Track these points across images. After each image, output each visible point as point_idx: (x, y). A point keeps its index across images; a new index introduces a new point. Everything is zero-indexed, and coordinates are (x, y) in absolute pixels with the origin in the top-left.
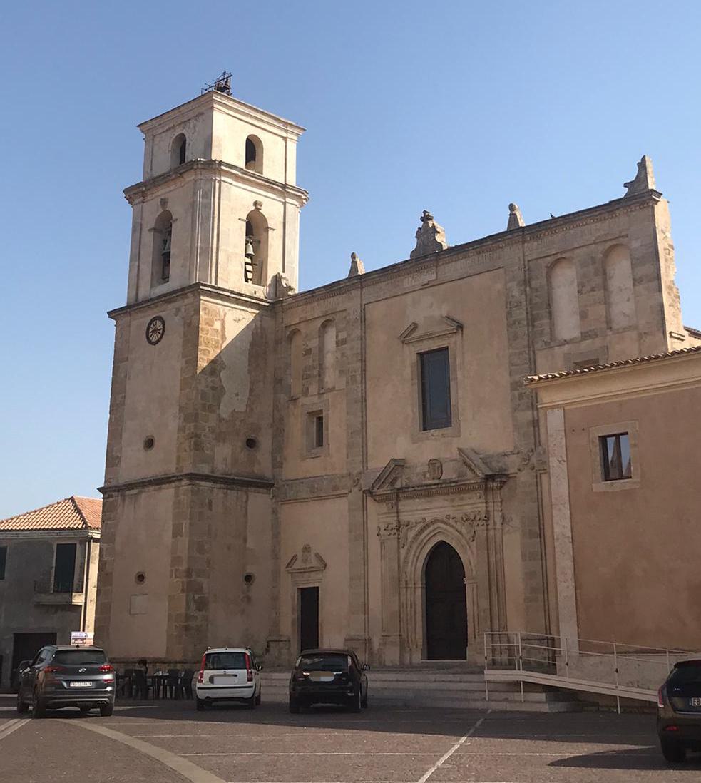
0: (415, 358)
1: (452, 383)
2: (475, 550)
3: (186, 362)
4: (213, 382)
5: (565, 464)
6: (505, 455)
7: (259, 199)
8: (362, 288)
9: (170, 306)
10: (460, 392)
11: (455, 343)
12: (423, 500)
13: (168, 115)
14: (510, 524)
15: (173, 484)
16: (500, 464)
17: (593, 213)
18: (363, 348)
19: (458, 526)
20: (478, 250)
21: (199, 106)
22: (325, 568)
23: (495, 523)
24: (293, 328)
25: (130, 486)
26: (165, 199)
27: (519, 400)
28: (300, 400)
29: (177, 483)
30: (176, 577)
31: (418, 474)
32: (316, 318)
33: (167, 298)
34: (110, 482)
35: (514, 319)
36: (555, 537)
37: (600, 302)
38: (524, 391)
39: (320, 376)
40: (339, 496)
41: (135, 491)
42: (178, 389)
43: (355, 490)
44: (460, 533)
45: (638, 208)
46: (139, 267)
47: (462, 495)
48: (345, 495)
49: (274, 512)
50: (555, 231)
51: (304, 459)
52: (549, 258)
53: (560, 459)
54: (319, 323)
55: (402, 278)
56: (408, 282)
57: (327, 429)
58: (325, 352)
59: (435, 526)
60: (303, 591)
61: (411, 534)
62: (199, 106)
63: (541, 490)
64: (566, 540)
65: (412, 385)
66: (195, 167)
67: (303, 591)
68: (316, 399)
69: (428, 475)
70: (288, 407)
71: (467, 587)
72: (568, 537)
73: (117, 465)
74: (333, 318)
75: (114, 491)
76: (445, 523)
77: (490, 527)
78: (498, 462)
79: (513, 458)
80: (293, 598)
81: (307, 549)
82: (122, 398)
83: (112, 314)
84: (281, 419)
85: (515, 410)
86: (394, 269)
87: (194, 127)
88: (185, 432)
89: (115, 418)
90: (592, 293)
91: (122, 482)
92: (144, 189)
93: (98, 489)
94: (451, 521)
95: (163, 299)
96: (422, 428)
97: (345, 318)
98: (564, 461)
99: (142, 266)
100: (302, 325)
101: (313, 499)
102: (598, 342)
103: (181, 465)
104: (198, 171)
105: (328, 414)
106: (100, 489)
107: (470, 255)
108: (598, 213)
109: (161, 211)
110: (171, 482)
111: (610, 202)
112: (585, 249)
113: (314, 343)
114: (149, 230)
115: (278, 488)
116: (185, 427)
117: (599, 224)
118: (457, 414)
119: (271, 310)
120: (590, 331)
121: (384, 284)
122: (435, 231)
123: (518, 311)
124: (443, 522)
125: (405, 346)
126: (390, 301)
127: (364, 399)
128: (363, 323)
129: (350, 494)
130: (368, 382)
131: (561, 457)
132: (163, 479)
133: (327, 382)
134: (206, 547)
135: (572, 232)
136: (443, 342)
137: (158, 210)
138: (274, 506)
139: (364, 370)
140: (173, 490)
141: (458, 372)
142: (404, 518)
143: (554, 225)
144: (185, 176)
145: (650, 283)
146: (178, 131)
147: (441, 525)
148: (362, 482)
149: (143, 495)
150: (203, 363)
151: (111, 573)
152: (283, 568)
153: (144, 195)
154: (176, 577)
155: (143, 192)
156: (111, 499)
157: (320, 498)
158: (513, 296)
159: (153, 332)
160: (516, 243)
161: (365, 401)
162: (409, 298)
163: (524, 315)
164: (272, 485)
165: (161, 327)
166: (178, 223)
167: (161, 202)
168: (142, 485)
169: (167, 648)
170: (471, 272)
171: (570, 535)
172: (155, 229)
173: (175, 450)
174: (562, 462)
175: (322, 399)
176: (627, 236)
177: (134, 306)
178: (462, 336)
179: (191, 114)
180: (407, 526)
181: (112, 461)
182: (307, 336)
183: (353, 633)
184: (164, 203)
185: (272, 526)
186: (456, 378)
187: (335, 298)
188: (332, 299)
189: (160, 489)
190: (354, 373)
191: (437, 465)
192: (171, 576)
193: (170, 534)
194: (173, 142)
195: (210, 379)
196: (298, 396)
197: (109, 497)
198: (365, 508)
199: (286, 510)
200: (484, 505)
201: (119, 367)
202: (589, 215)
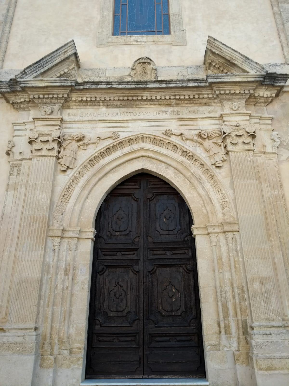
19: (189, 146)
59: (136, 147)
94: (175, 140)
147: (149, 146)
180: (78, 141)
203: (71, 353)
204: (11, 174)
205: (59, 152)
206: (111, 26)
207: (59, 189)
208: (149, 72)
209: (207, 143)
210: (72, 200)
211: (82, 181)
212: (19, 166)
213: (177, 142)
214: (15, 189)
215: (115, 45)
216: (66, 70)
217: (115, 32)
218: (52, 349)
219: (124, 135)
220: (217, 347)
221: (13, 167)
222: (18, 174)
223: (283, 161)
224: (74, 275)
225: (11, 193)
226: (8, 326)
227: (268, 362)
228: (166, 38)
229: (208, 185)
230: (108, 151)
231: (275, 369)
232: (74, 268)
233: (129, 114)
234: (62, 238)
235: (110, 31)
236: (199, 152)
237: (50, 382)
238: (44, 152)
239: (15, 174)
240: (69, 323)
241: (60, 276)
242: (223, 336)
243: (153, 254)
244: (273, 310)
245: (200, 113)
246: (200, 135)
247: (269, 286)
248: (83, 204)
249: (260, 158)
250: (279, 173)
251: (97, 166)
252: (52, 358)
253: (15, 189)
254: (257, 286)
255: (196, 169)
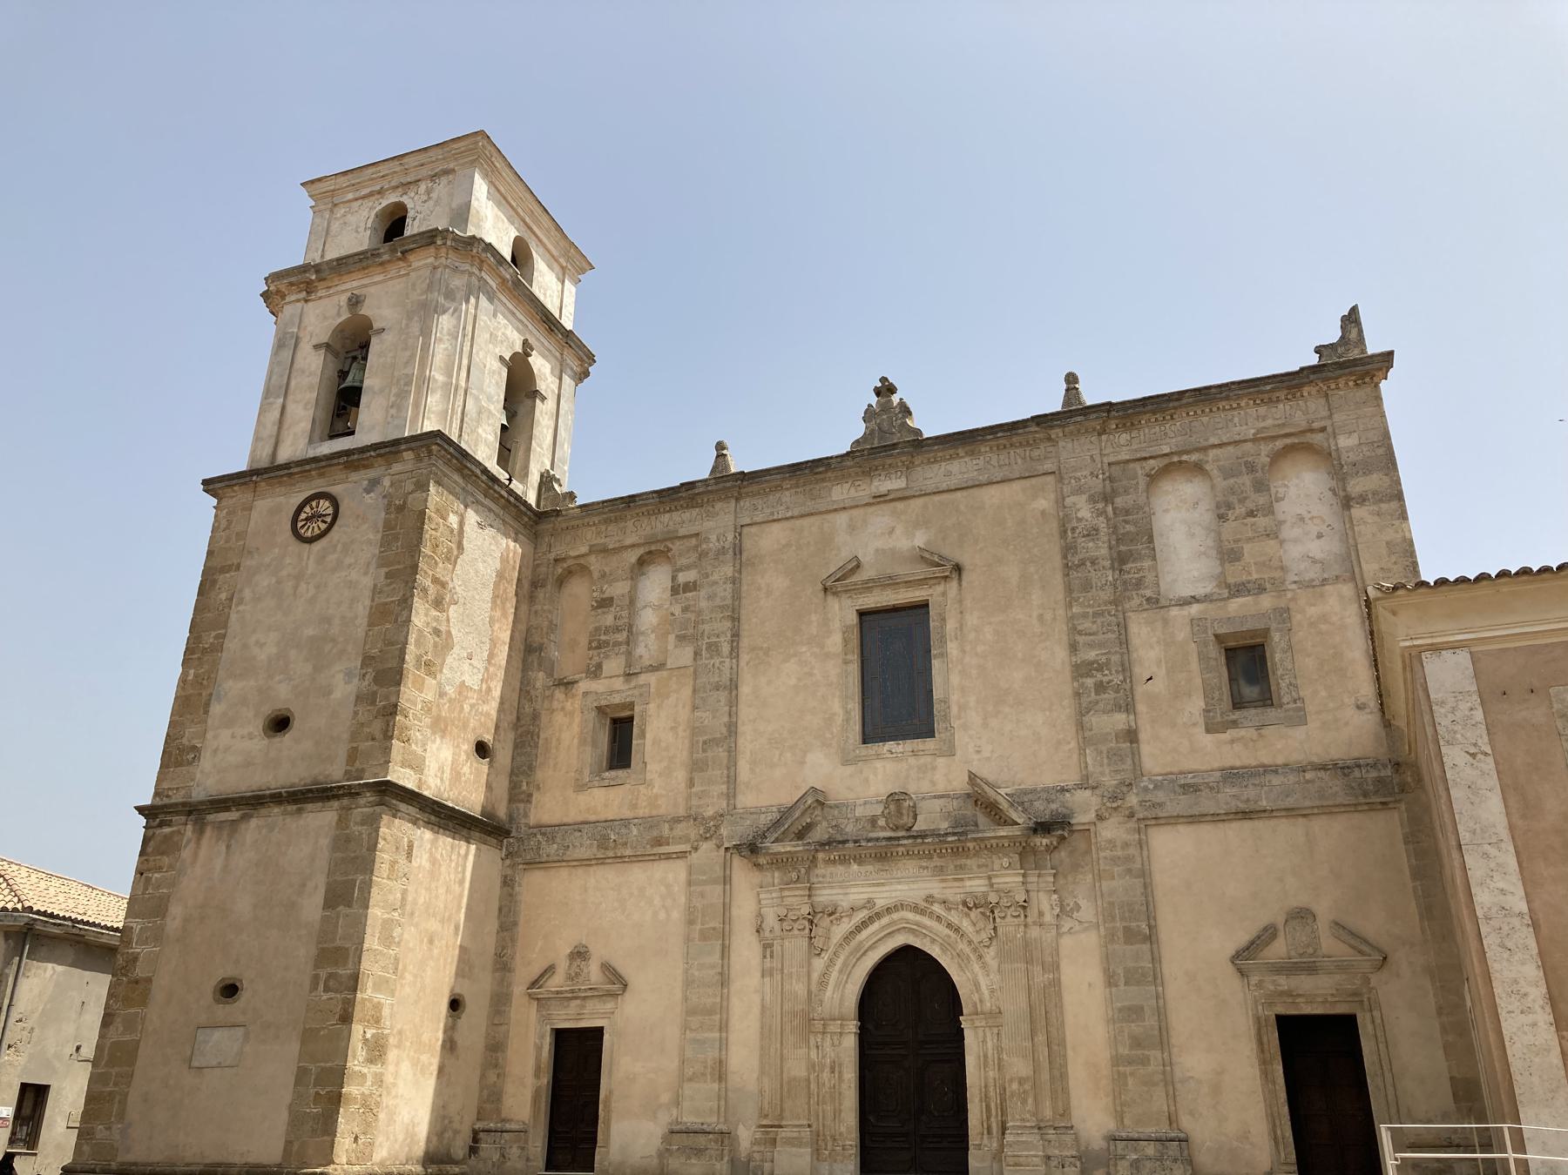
0: (853, 619)
1: (936, 663)
2: (993, 964)
3: (388, 576)
4: (437, 619)
5: (1490, 760)
6: (1063, 790)
7: (532, 341)
8: (737, 500)
9: (354, 476)
10: (955, 679)
11: (944, 594)
12: (870, 868)
13: (372, 170)
14: (1075, 915)
15: (336, 804)
16: (1054, 806)
17: (1258, 386)
18: (737, 596)
19: (954, 917)
20: (1001, 441)
21: (444, 159)
22: (624, 991)
23: (1041, 914)
24: (570, 562)
25: (222, 804)
26: (357, 296)
27: (1097, 693)
28: (580, 684)
29: (345, 801)
30: (327, 989)
31: (857, 820)
32: (627, 547)
33: (353, 460)
34: (168, 796)
35: (1081, 556)
36: (1479, 913)
37: (1268, 535)
38: (1105, 679)
39: (628, 644)
40: (668, 857)
41: (234, 815)
42: (362, 622)
43: (706, 846)
44: (957, 930)
45: (1351, 383)
46: (283, 408)
47: (963, 861)
48: (682, 855)
49: (507, 882)
50: (1172, 416)
51: (580, 787)
52: (1152, 462)
53: (1472, 750)
54: (632, 557)
55: (829, 484)
56: (841, 492)
57: (643, 735)
58: (639, 604)
59: (895, 916)
60: (562, 1038)
61: (840, 930)
62: (444, 159)
63: (1148, 857)
64: (1516, 922)
65: (846, 662)
66: (439, 242)
67: (562, 1038)
68: (619, 684)
69: (881, 822)
70: (552, 695)
71: (967, 1033)
72: (1520, 914)
73: (190, 763)
74: (666, 546)
75: (177, 813)
76: (922, 912)
77: (1029, 920)
78: (1049, 801)
79: (1083, 796)
80: (539, 1049)
81: (580, 954)
82: (216, 637)
83: (210, 485)
84: (535, 716)
85: (1081, 713)
86: (817, 467)
87: (428, 192)
88: (373, 703)
89: (196, 676)
90: (1251, 520)
91: (198, 795)
92: (314, 277)
93: (136, 808)
94: (937, 908)
95: (341, 460)
96: (1232, 644)
97: (696, 547)
98: (1486, 754)
99: (290, 407)
100: (592, 559)
101: (601, 861)
102: (1266, 602)
103: (357, 765)
104: (443, 252)
105: (645, 711)
106: (141, 810)
107: (983, 449)
108: (1268, 387)
109: (346, 315)
110: (328, 798)
111: (1302, 369)
112: (1230, 449)
113: (619, 589)
114: (317, 347)
115: (520, 840)
116: (374, 693)
117: (1263, 410)
118: (946, 718)
119: (532, 526)
120: (1249, 582)
121: (787, 493)
122: (906, 411)
123: (1091, 544)
124: (916, 909)
125: (830, 598)
126: (798, 522)
127: (733, 686)
128: (738, 556)
129: (694, 855)
130: (744, 658)
131: (1475, 745)
132: (310, 791)
133: (641, 657)
134: (397, 932)
135: (1205, 419)
136: (917, 593)
137: (339, 314)
138: (509, 872)
139: (736, 635)
140: (335, 813)
141: (949, 645)
142: (824, 896)
143: (1176, 404)
144: (411, 257)
145: (1383, 505)
146: (392, 198)
147: (910, 916)
148: (724, 831)
149: (254, 822)
150: (534, 505)
151: (149, 980)
152: (519, 990)
153: (309, 288)
154: (327, 989)
155: (309, 283)
156: (167, 830)
157: (620, 859)
158: (1080, 520)
159: (307, 519)
160: (1086, 431)
161: (737, 688)
162: (842, 519)
163: (1104, 551)
164: (507, 833)
165: (330, 511)
166: (388, 337)
167: (350, 300)
168: (254, 802)
169: (288, 1143)
170: (984, 478)
171: (1525, 908)
172: (327, 346)
173: (346, 736)
174: (1480, 756)
175: (633, 685)
176: (1323, 429)
177: (266, 470)
178: (960, 584)
179: (425, 172)
180: (830, 915)
181: (177, 754)
182: (603, 575)
183: (689, 1120)
184: (355, 302)
185: (500, 910)
186: (943, 655)
187: (675, 514)
188: (667, 515)
189: (300, 811)
190: (714, 639)
191: (906, 804)
192: (314, 986)
193: (319, 898)
194: (377, 216)
195: (434, 613)
196: (577, 677)
197: (161, 825)
198: (726, 880)
199: (533, 884)
200: (1021, 879)
201: (214, 582)
202: (1246, 391)
203: (843, 1149)
204: (765, 957)
205: (811, 930)
206: (857, 728)
207: (815, 976)
208: (905, 812)
209: (974, 914)
210: (830, 988)
211: (839, 963)
212: (771, 946)
213: (939, 911)
214: (771, 975)
215: (866, 760)
216: (809, 820)
217: (866, 739)
218: (826, 1145)
219: (881, 903)
220: (979, 1147)
221: (765, 947)
222: (772, 957)
223: (1064, 933)
224: (840, 1072)
225: (767, 979)
226: (784, 1123)
227: (1016, 1159)
228: (929, 744)
229: (977, 967)
230: (864, 924)
231: (1022, 1166)
232: (840, 1065)
233: (884, 873)
234: (824, 1033)
235: (858, 738)
236: (965, 925)
237: (827, 1172)
238: (796, 932)
239: (768, 956)
240: (840, 1122)
241: (826, 1075)
242: (985, 1137)
243: (1183, 786)
244: (1029, 1111)
245: (1164, 511)
246: (965, 903)
247: (1027, 1087)
248: (843, 991)
249: (1034, 932)
250: (1057, 950)
251: (853, 943)
252: (827, 1152)
253: (771, 975)
254: (1015, 1086)
255: (962, 946)
